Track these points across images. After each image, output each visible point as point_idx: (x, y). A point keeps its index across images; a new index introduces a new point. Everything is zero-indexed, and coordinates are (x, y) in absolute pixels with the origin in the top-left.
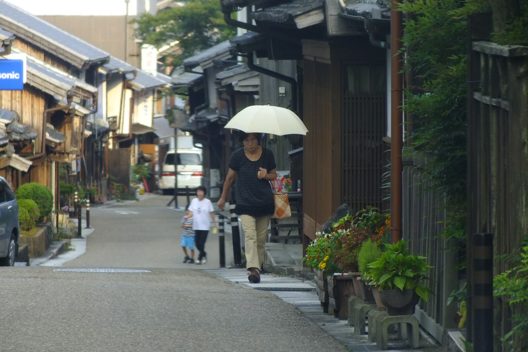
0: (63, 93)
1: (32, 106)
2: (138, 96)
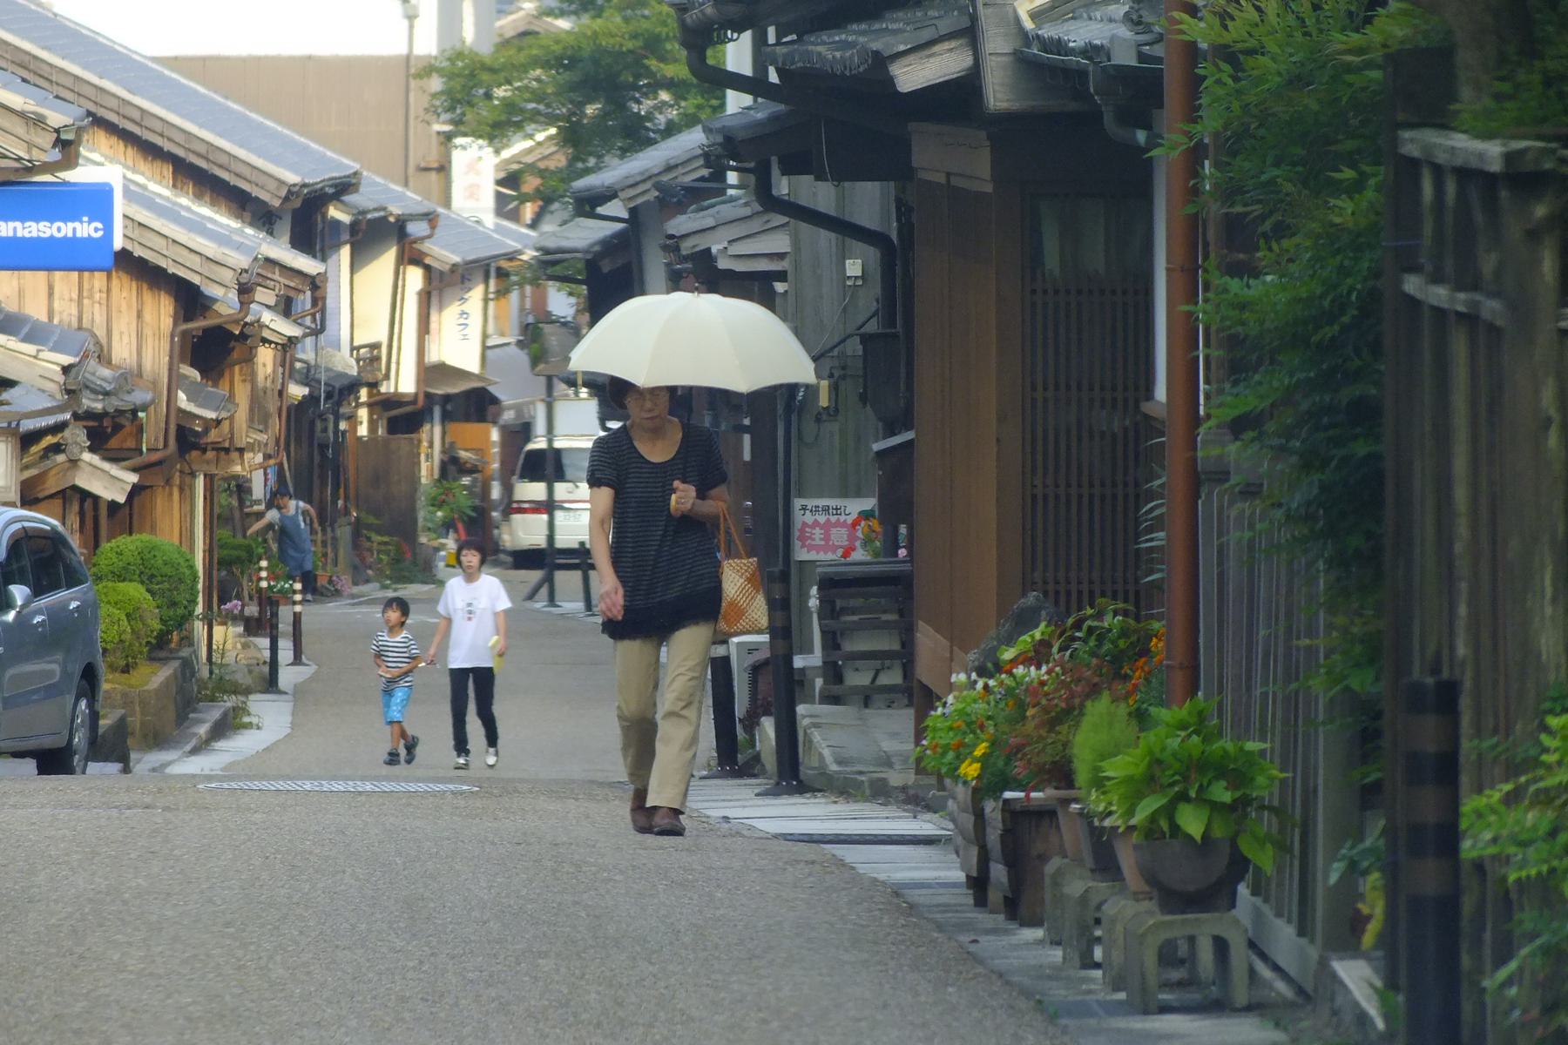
0: (228, 277)
2: (442, 285)
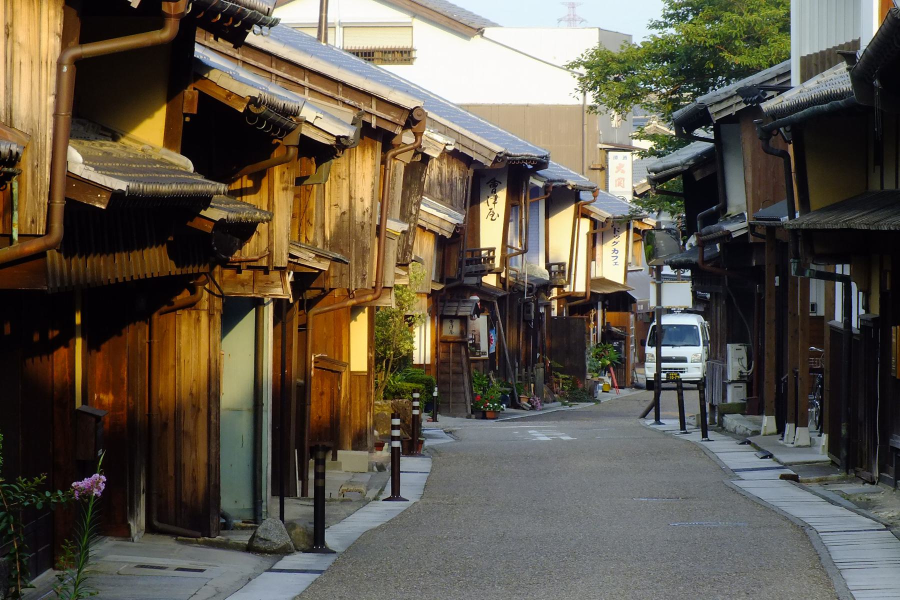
2: (601, 231)
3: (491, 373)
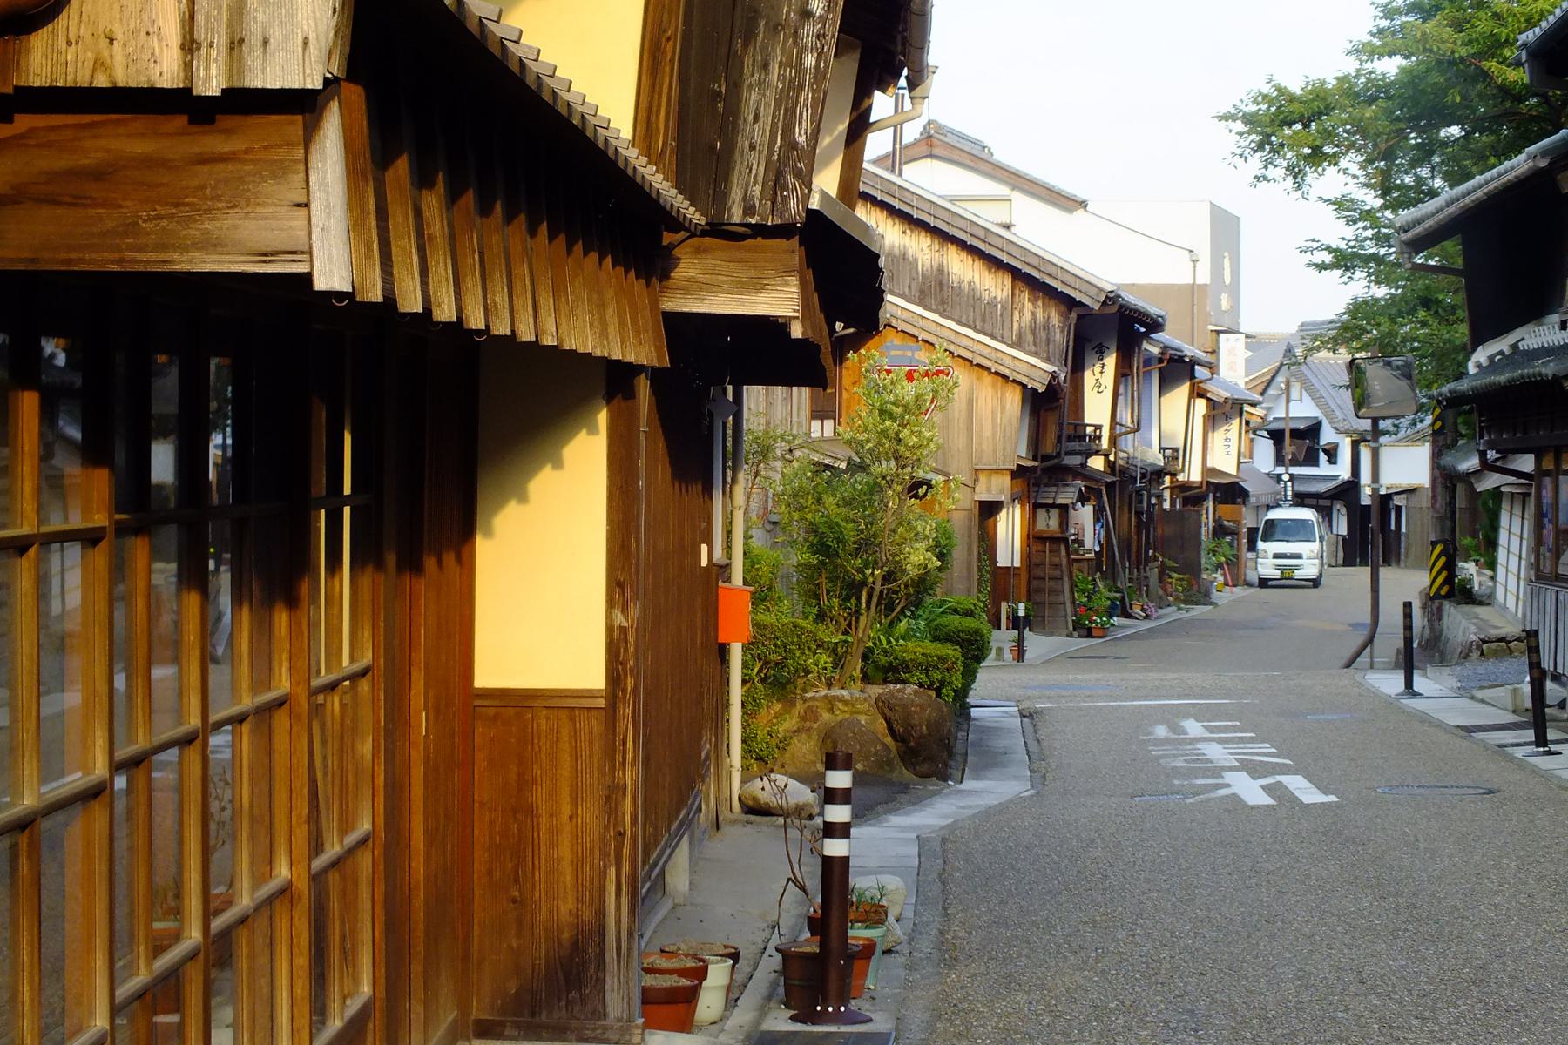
1: (418, 213)
3: (1098, 575)
